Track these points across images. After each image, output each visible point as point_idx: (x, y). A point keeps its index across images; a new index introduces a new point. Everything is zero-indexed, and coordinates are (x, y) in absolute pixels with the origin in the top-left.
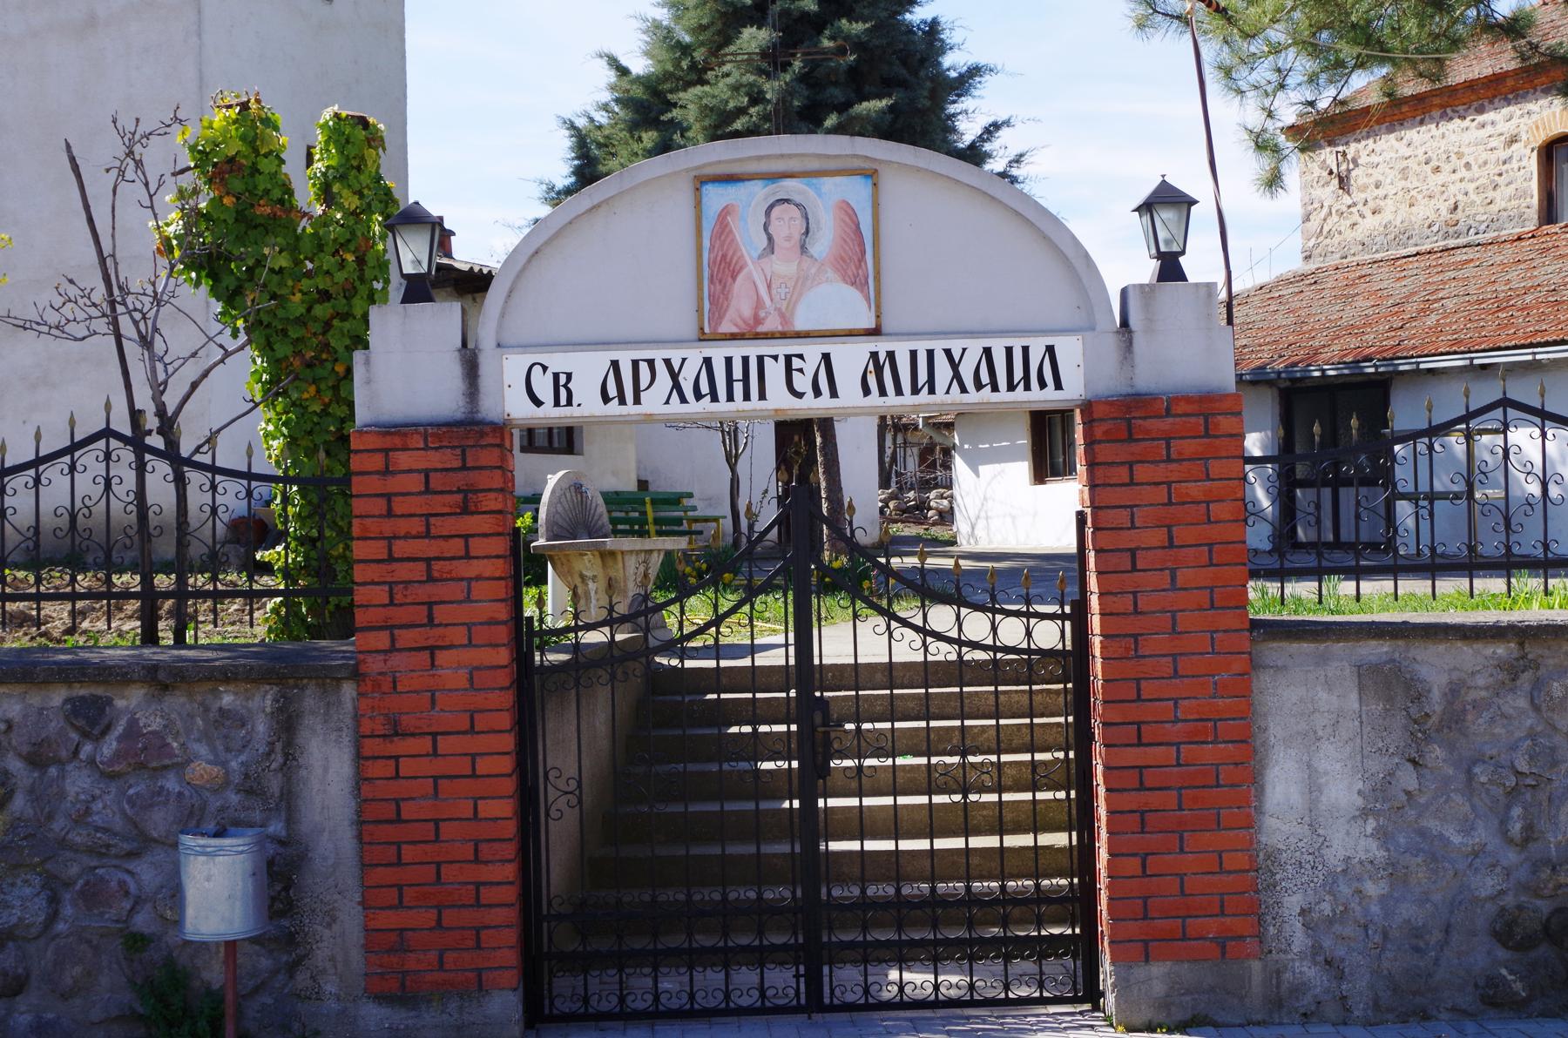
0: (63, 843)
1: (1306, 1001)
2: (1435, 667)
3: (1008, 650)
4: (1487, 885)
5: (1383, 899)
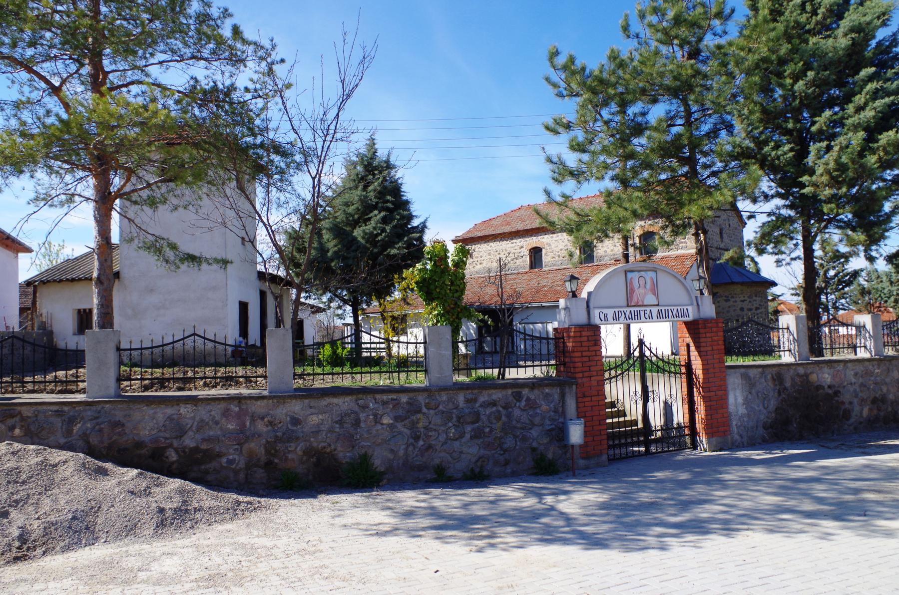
0: (515, 427)
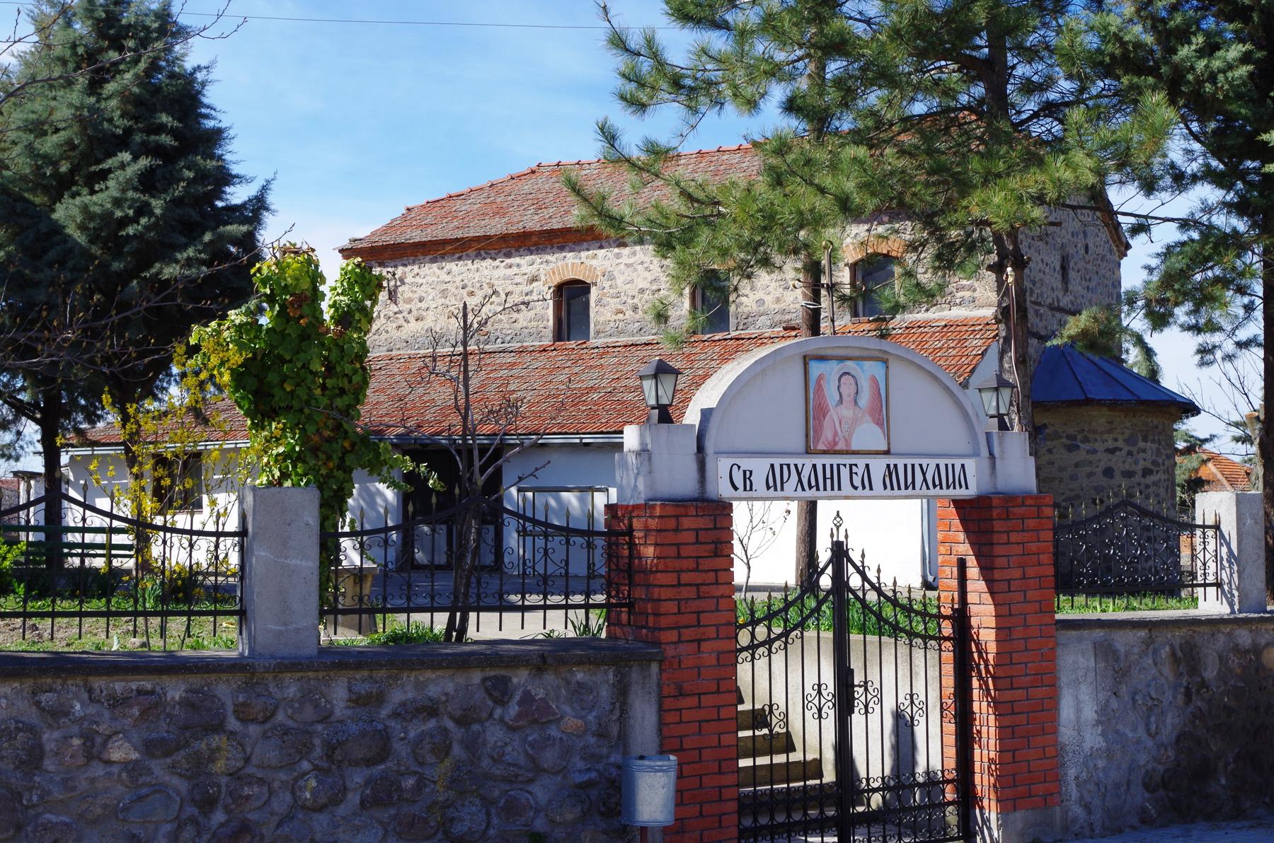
1: (1076, 828)
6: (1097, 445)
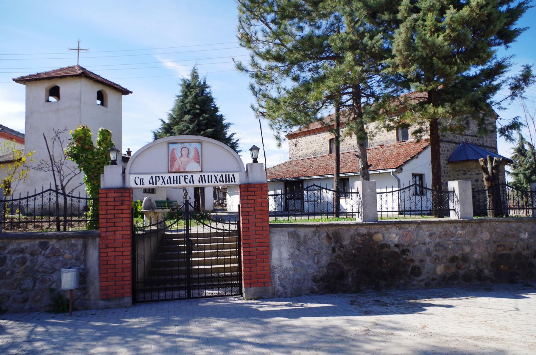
0: (37, 271)
1: (279, 294)
2: (302, 232)
3: (226, 230)
4: (311, 271)
5: (293, 274)
6: (473, 173)
